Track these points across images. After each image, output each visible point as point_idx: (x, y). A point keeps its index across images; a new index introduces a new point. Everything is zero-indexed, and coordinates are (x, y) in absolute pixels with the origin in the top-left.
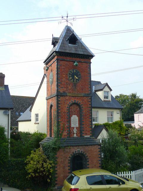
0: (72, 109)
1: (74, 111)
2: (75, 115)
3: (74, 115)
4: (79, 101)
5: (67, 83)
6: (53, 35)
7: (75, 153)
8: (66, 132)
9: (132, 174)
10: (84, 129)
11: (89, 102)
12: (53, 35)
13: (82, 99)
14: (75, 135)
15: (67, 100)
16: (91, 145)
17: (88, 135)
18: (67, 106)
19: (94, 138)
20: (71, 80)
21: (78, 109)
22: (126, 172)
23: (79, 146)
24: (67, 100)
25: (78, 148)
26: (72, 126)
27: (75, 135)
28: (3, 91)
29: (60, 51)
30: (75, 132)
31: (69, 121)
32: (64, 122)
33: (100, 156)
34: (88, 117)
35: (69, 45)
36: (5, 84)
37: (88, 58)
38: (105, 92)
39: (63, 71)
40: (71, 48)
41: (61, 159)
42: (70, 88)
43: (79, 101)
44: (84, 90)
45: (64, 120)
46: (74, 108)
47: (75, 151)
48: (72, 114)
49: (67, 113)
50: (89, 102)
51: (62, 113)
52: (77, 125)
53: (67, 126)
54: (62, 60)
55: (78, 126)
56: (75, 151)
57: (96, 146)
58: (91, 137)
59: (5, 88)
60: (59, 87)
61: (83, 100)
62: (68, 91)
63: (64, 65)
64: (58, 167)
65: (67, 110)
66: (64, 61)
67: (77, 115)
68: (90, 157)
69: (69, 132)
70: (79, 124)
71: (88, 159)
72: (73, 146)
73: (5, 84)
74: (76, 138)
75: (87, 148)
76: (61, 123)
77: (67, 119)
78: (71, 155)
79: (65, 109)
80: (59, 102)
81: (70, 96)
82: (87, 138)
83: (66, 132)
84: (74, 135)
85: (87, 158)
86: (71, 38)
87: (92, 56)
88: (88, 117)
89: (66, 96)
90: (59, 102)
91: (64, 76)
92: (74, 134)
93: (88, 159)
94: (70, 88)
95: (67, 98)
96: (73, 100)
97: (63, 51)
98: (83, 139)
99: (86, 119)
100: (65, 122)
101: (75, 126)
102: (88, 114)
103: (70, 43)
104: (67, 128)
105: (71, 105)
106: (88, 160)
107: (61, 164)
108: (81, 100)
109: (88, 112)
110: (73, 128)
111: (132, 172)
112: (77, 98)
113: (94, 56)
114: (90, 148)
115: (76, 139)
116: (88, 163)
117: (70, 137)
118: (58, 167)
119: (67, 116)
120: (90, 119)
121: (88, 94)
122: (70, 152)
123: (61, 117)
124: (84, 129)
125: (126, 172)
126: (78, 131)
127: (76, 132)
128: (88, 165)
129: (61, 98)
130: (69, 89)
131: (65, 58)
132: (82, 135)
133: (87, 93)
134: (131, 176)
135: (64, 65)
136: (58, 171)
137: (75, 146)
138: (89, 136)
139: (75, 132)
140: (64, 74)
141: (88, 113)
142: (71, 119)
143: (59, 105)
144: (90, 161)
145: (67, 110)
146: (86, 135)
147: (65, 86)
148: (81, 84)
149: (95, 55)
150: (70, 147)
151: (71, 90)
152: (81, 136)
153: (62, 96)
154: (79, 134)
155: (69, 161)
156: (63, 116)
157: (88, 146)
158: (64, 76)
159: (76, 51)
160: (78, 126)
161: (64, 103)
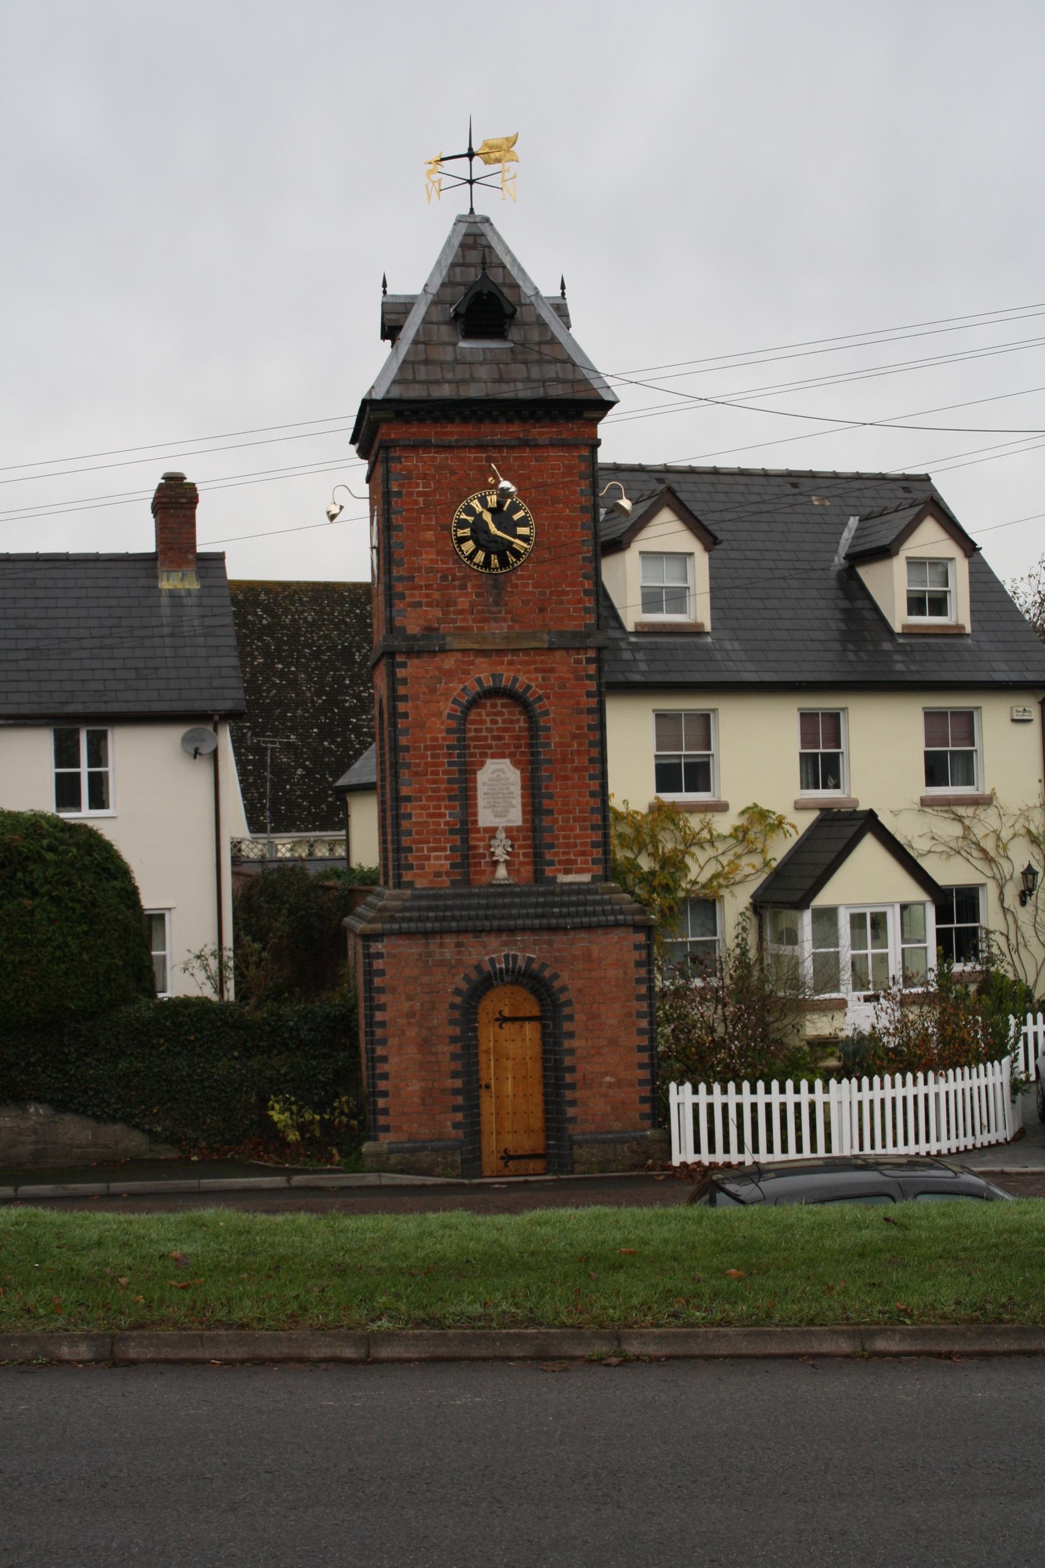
0: (483, 722)
1: (494, 738)
2: (502, 756)
3: (493, 756)
4: (522, 678)
5: (444, 578)
6: (385, 285)
7: (487, 967)
8: (447, 858)
9: (833, 1097)
10: (557, 837)
11: (589, 677)
12: (385, 285)
13: (542, 662)
14: (502, 872)
15: (449, 674)
16: (589, 928)
17: (580, 871)
18: (447, 708)
19: (613, 891)
20: (474, 553)
21: (518, 721)
22: (915, 1079)
23: (512, 931)
24: (449, 674)
25: (505, 944)
26: (485, 818)
27: (502, 872)
28: (185, 601)
29: (396, 393)
30: (500, 854)
31: (465, 795)
32: (429, 798)
33: (643, 989)
34: (575, 769)
35: (463, 344)
36: (203, 545)
37: (579, 415)
38: (914, 563)
39: (420, 511)
40: (478, 366)
41: (410, 998)
42: (463, 603)
43: (522, 677)
44: (553, 611)
45: (434, 790)
46: (490, 719)
47: (492, 961)
48: (484, 755)
49: (449, 747)
50: (589, 677)
51: (418, 748)
52: (515, 817)
53: (447, 823)
54: (415, 447)
55: (519, 822)
56: (492, 961)
57: (614, 936)
58: (601, 885)
59: (200, 577)
60: (399, 605)
61: (551, 670)
62: (454, 621)
63: (424, 476)
64: (393, 1041)
65: (449, 731)
66: (426, 446)
67: (511, 755)
68: (580, 991)
69: (466, 857)
70: (524, 812)
71: (568, 1003)
72: (478, 932)
73: (203, 545)
74: (503, 890)
75: (560, 941)
76: (415, 808)
77: (450, 781)
78: (466, 978)
79: (439, 729)
80: (402, 690)
81: (463, 651)
82: (579, 889)
83: (447, 858)
84: (494, 872)
85: (563, 998)
86: (481, 296)
87: (605, 406)
88: (575, 769)
89: (443, 650)
90: (402, 690)
91: (429, 535)
92: (495, 863)
93: (568, 1003)
94: (463, 603)
95: (449, 662)
96: (483, 673)
97: (415, 392)
98: (543, 894)
99: (566, 778)
100: (440, 799)
101: (500, 823)
102: (579, 752)
103: (468, 335)
104: (452, 832)
105: (474, 703)
106: (566, 1011)
107: (409, 1024)
108: (537, 670)
109: (574, 736)
110: (492, 831)
111: (833, 1082)
112: (511, 663)
113: (610, 404)
114: (581, 942)
115: (502, 895)
116: (567, 1026)
117: (468, 882)
118: (390, 1042)
119: (450, 764)
120: (592, 777)
121: (575, 635)
122: (459, 962)
123: (417, 774)
124: (557, 837)
125: (915, 1079)
126: (521, 847)
127: (508, 853)
128: (571, 1035)
129: (414, 662)
130: (461, 612)
131: (429, 431)
132: (543, 871)
133: (571, 625)
134: (826, 1105)
135: (424, 476)
136: (393, 1060)
137: (490, 931)
138: (586, 878)
139: (500, 854)
140: (428, 528)
141: (580, 744)
142: (475, 781)
143: (402, 707)
144: (579, 1017)
145: (449, 731)
146: (567, 872)
147: (437, 595)
148: (530, 577)
149: (619, 390)
150: (461, 938)
151: (470, 617)
152: (538, 876)
153: (419, 654)
154: (527, 863)
155: (457, 1014)
156: (427, 764)
157: (564, 930)
158: (429, 535)
159: (500, 380)
160: (519, 822)
161: (433, 690)
